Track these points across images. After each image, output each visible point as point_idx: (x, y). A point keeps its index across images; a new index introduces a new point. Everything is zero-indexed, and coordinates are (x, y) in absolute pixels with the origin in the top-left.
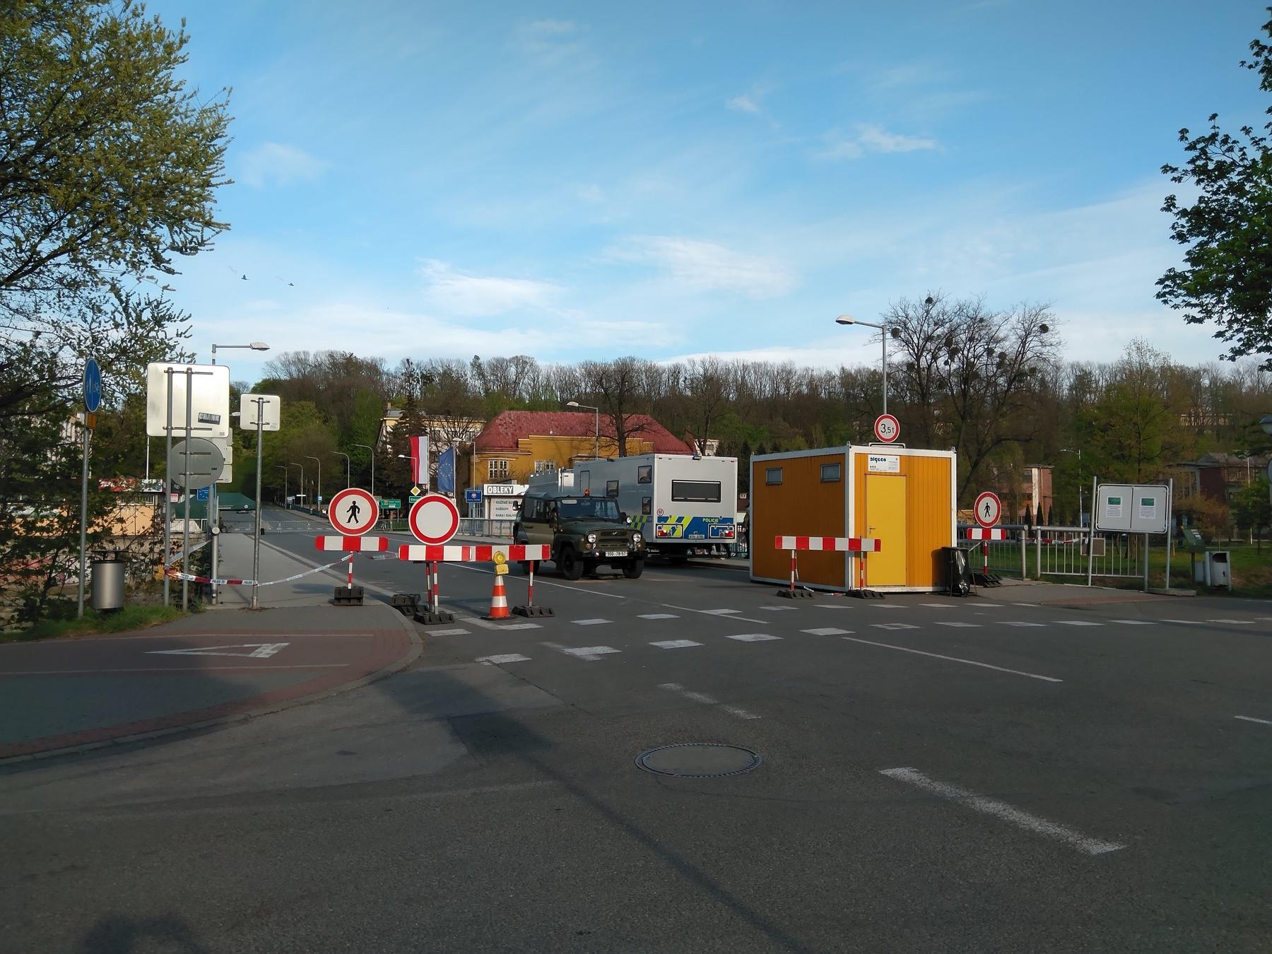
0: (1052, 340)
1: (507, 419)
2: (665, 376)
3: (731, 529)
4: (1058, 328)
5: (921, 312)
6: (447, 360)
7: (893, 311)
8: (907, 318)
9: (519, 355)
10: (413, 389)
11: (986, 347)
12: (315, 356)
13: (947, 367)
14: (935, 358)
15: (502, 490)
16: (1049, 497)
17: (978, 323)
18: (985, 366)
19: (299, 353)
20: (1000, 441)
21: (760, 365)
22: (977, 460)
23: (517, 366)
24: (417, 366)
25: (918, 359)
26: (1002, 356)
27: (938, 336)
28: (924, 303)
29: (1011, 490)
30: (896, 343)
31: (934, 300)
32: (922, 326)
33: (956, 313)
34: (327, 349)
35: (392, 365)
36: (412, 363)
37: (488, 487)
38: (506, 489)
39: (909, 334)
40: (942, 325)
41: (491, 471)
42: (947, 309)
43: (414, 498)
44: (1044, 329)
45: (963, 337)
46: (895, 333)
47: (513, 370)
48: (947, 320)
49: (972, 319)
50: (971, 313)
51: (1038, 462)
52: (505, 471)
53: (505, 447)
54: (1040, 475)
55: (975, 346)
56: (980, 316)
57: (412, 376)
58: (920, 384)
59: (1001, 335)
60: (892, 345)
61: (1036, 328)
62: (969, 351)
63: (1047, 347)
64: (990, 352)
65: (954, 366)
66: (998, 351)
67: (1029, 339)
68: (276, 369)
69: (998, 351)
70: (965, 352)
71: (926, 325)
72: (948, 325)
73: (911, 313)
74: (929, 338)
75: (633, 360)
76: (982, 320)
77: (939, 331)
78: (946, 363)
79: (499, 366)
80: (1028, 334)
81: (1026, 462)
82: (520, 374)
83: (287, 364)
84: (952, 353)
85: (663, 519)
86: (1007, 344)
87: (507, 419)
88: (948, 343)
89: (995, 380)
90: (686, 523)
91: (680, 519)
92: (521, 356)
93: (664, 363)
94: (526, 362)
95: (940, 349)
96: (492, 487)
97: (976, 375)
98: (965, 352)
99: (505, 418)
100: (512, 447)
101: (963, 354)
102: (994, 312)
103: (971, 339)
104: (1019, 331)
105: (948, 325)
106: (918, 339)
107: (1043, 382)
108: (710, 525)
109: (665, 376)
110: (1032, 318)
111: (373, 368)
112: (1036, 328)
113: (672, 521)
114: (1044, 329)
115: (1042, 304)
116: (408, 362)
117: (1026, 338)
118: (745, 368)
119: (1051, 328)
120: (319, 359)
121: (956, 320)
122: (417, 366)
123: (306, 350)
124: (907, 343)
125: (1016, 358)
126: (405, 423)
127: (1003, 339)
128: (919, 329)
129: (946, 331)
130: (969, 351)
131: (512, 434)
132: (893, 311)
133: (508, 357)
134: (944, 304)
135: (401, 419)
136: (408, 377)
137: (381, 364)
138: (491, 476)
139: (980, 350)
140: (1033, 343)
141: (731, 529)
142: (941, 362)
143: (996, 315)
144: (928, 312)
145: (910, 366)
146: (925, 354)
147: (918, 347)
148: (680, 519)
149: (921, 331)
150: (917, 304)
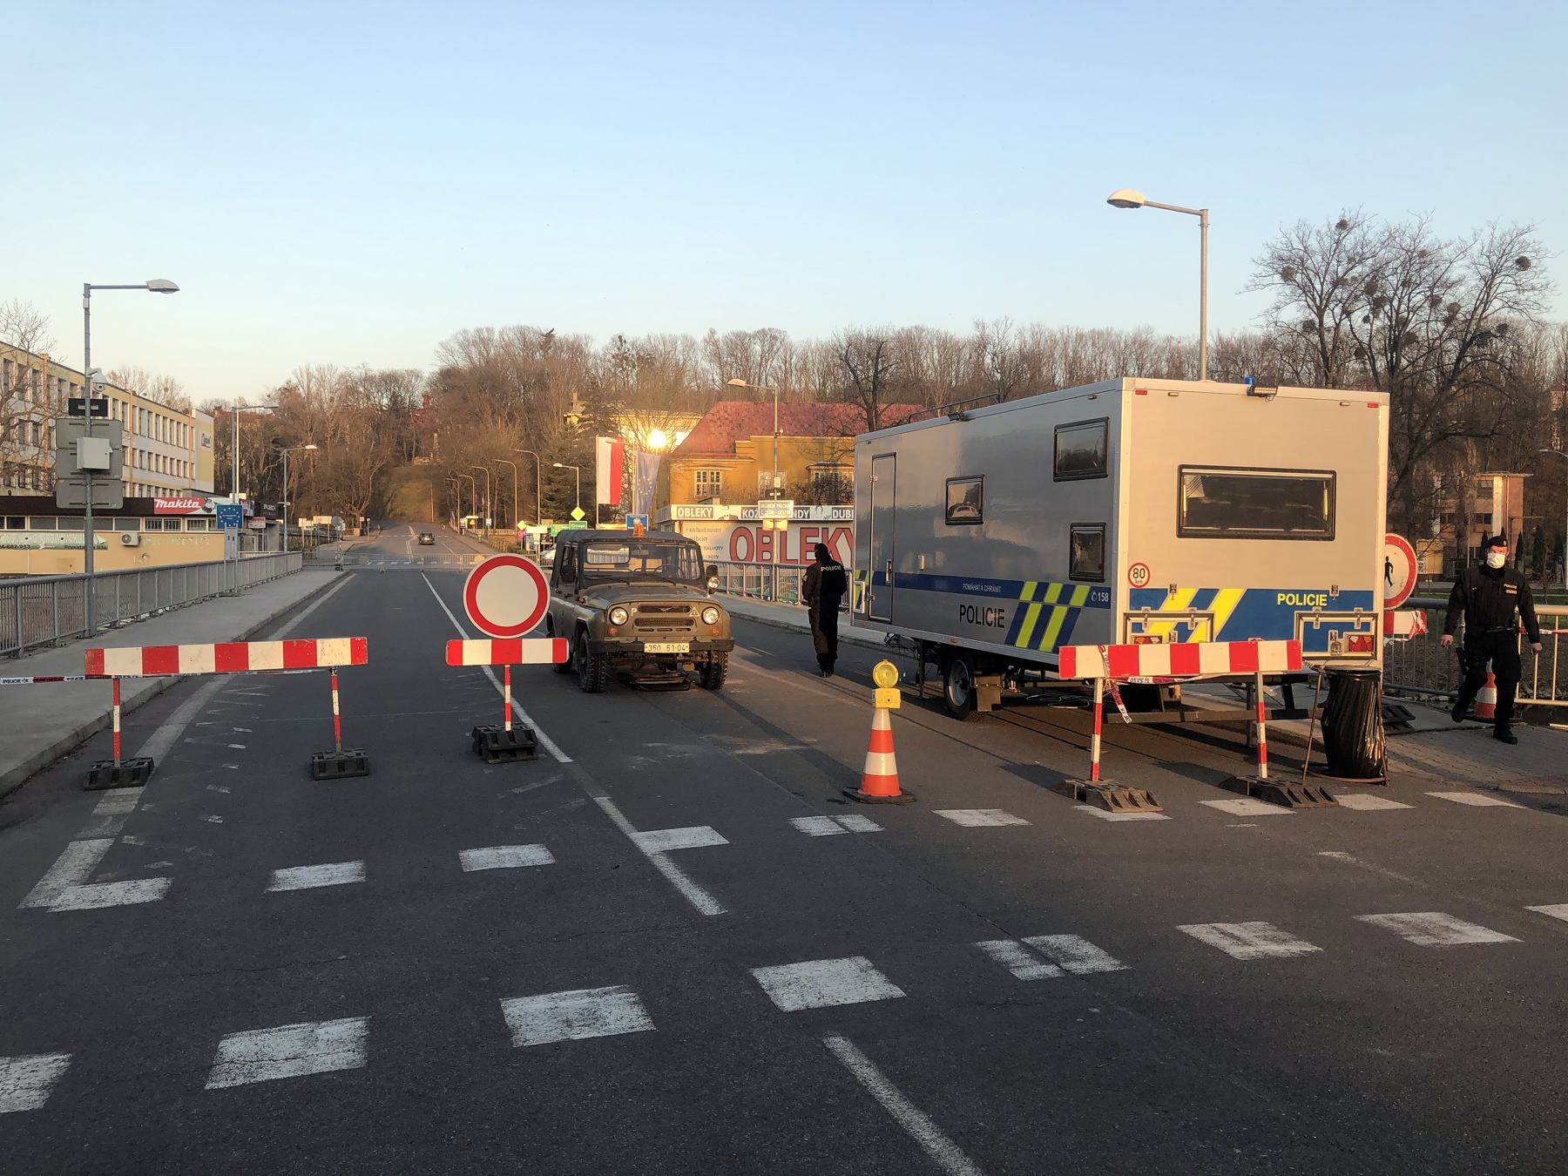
0: (1535, 281)
1: (722, 413)
2: (966, 353)
3: (1366, 626)
4: (1546, 262)
5: (1327, 242)
6: (670, 335)
7: (1284, 240)
8: (1306, 252)
9: (767, 328)
10: (628, 376)
11: (1429, 293)
12: (501, 334)
13: (1368, 326)
14: (1347, 313)
15: (697, 512)
16: (1518, 518)
17: (1417, 258)
18: (1425, 325)
19: (482, 330)
20: (1445, 436)
21: (1100, 334)
22: (1407, 466)
23: (763, 341)
24: (633, 344)
25: (1320, 315)
26: (1454, 308)
27: (1354, 279)
28: (1333, 228)
29: (1461, 507)
30: (1288, 290)
31: (1351, 224)
32: (1329, 264)
33: (1383, 243)
34: (516, 325)
35: (599, 344)
36: (625, 341)
37: (678, 508)
38: (703, 512)
39: (1308, 276)
40: (1360, 262)
41: (698, 486)
42: (1370, 237)
43: (576, 523)
44: (1523, 263)
45: (1394, 280)
46: (1287, 275)
47: (757, 348)
48: (1367, 255)
49: (1407, 251)
50: (1407, 241)
51: (1506, 467)
52: (718, 486)
53: (717, 452)
54: (1505, 488)
55: (1410, 293)
56: (1421, 247)
57: (626, 359)
58: (1323, 353)
59: (1453, 275)
60: (1276, 290)
61: (1509, 264)
62: (1400, 303)
63: (1526, 293)
64: (1434, 301)
65: (1378, 324)
66: (1448, 299)
67: (1497, 281)
68: (452, 353)
69: (1448, 299)
70: (1395, 303)
71: (1334, 262)
72: (1370, 261)
73: (1313, 243)
74: (1338, 282)
75: (920, 329)
76: (1423, 254)
77: (1358, 270)
78: (1366, 319)
79: (739, 344)
80: (1496, 273)
81: (1484, 469)
82: (767, 355)
83: (465, 345)
84: (1377, 305)
85: (1148, 598)
86: (1462, 289)
87: (722, 413)
88: (1370, 289)
89: (1441, 344)
90: (1223, 607)
91: (1204, 598)
92: (770, 329)
93: (962, 331)
94: (775, 338)
95: (1357, 298)
96: (684, 508)
97: (1412, 338)
98: (1395, 303)
99: (718, 412)
100: (726, 452)
101: (1391, 306)
102: (1444, 240)
103: (1406, 284)
104: (1481, 268)
105: (1370, 261)
106: (1322, 284)
107: (1518, 352)
108: (1301, 616)
109: (966, 353)
110: (1504, 247)
111: (576, 349)
112: (1509, 264)
113: (1178, 602)
114: (1523, 263)
115: (1522, 225)
116: (621, 340)
117: (1493, 278)
118: (1080, 337)
119: (1534, 263)
120: (506, 338)
121: (1384, 254)
122: (633, 345)
123: (490, 326)
124: (1306, 289)
125: (1476, 309)
126: (588, 420)
127: (1459, 281)
128: (1323, 268)
129: (1367, 270)
130: (1400, 303)
131: (728, 434)
132: (1284, 240)
133: (750, 330)
134: (1365, 229)
135: (583, 413)
136: (621, 360)
137: (587, 344)
138: (698, 493)
139: (1418, 298)
140: (1504, 285)
141: (1366, 626)
142: (1357, 317)
143: (1446, 246)
144: (1338, 242)
145: (1308, 326)
146: (1332, 306)
147: (1320, 297)
148: (1204, 598)
149: (1326, 272)
150: (1325, 229)
